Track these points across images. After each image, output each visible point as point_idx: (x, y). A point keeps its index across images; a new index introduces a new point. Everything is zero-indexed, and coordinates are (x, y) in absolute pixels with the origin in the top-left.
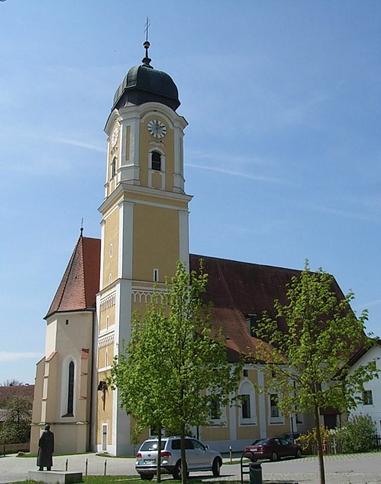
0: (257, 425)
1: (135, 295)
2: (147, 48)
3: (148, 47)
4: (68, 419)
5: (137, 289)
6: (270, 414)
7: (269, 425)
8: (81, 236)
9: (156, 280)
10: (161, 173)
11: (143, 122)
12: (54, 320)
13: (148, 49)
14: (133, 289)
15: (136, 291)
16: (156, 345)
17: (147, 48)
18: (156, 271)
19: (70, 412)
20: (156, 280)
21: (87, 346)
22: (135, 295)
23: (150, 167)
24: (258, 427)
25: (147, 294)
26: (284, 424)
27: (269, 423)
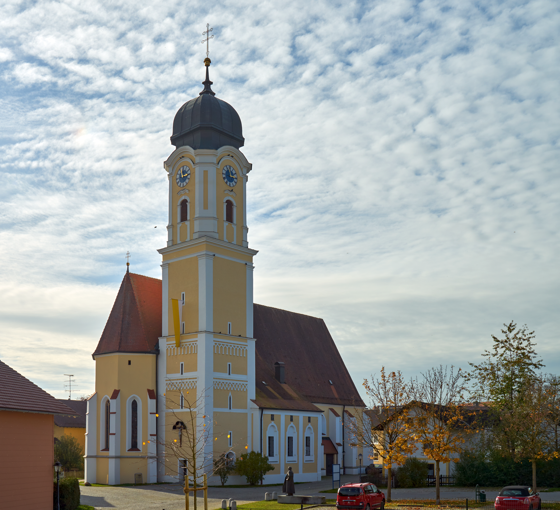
0: (297, 462)
1: (216, 346)
2: (207, 66)
3: (209, 66)
4: (105, 453)
5: (225, 342)
6: (305, 454)
7: (305, 462)
8: (128, 271)
9: (229, 333)
10: (233, 226)
11: (219, 167)
12: (283, 388)
13: (209, 67)
14: (214, 341)
15: (216, 343)
16: (406, 417)
17: (207, 66)
18: (230, 324)
19: (134, 447)
20: (229, 333)
21: (152, 387)
22: (216, 346)
23: (225, 219)
24: (298, 463)
25: (221, 346)
26: (313, 462)
27: (305, 461)
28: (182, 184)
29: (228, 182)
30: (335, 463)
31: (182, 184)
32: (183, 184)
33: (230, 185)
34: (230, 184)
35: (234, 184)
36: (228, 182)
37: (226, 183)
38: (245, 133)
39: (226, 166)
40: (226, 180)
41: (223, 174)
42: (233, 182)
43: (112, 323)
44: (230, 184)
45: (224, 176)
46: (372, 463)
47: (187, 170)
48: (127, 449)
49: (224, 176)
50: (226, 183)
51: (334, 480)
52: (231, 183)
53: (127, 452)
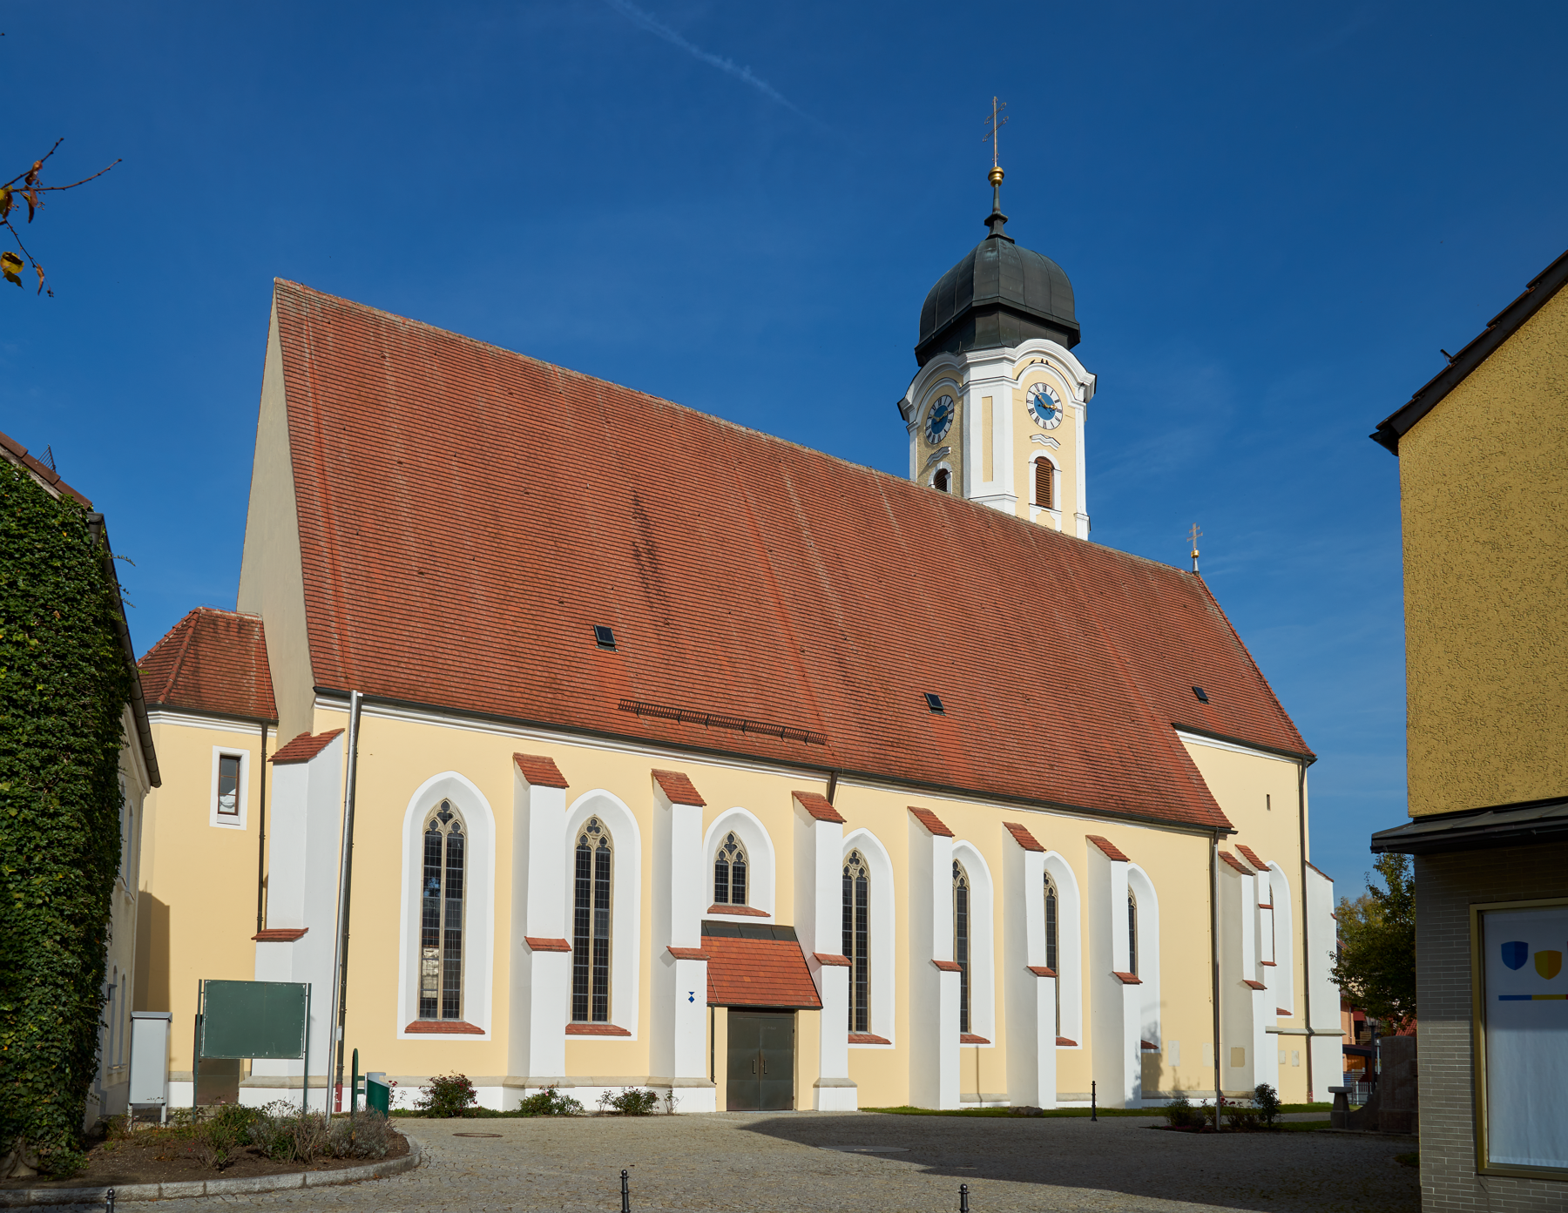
11: (1019, 387)
28: (937, 435)
29: (1041, 420)
30: (318, 700)
31: (937, 435)
32: (939, 436)
33: (1045, 427)
34: (1045, 424)
35: (1056, 423)
36: (1041, 420)
37: (1037, 420)
38: (1081, 339)
39: (1036, 385)
40: (1035, 415)
41: (1030, 411)
42: (1053, 420)
43: (342, 427)
44: (1045, 424)
45: (1032, 406)
46: (1417, 1015)
47: (946, 405)
48: (402, 1026)
49: (1032, 406)
50: (1037, 420)
51: (1496, 1157)
52: (1048, 422)
53: (401, 1035)
